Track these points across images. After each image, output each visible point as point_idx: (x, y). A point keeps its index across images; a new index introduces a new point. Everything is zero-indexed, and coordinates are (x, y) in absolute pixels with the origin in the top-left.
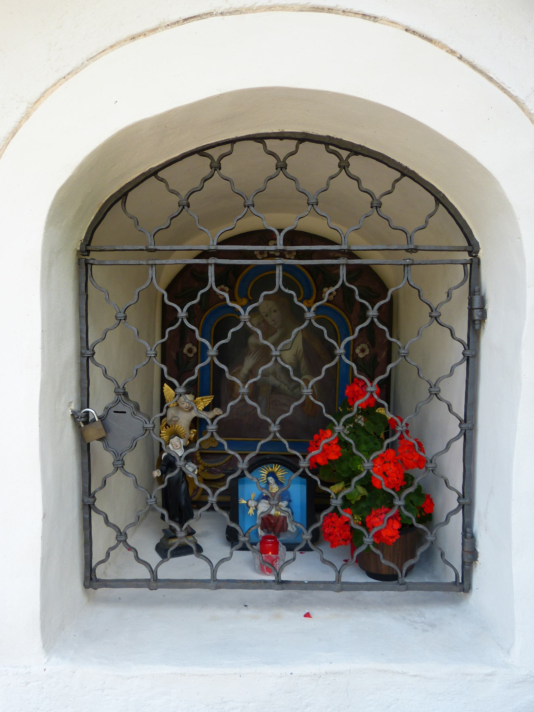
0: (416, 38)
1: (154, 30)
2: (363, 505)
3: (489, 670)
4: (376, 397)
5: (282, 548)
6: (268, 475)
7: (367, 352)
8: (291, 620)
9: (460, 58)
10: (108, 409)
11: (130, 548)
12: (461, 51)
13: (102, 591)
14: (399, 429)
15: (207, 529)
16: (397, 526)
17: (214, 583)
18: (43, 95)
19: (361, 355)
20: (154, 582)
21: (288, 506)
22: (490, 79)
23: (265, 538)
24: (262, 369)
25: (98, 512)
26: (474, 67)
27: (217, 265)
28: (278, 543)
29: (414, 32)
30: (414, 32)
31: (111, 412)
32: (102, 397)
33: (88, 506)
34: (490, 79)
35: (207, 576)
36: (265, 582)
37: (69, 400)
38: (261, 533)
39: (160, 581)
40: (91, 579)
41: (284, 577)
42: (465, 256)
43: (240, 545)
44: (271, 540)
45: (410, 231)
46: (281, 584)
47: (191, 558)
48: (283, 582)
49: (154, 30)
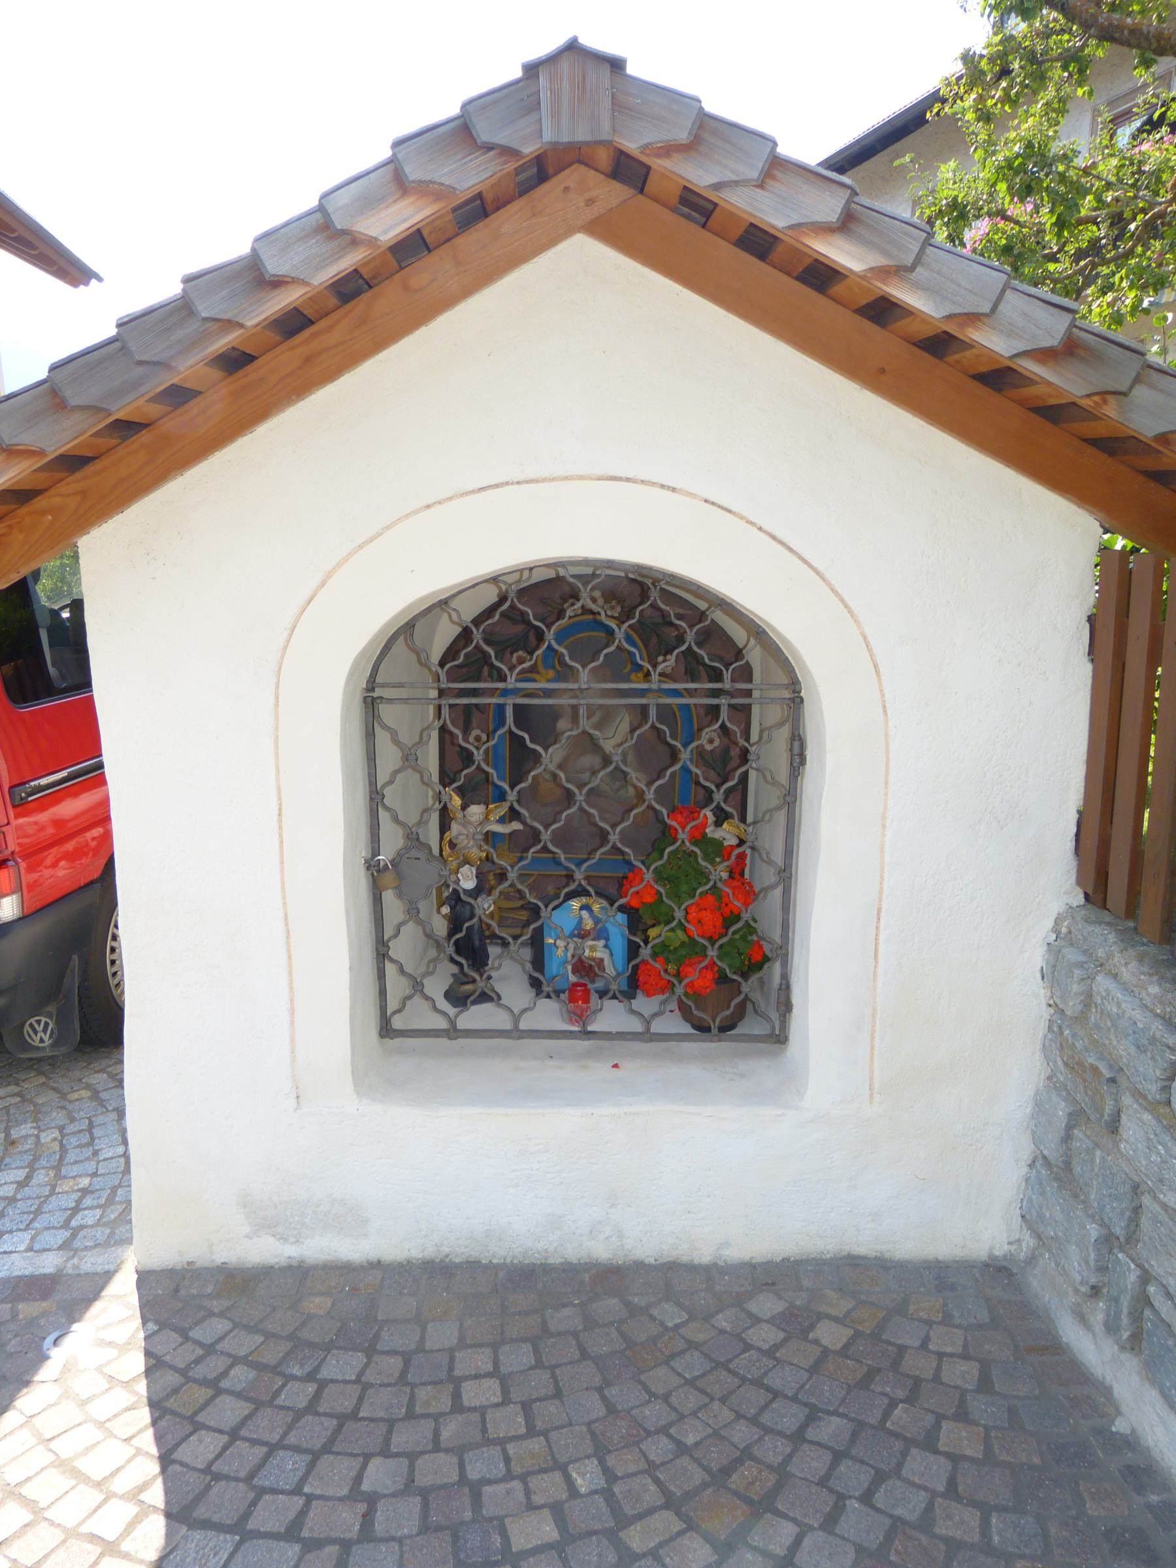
0: (715, 508)
1: (450, 499)
2: (683, 952)
3: (780, 1112)
4: (687, 844)
5: (594, 997)
6: (581, 908)
7: (717, 743)
8: (600, 1071)
9: (760, 529)
10: (399, 855)
11: (427, 998)
12: (760, 523)
13: (398, 1042)
14: (712, 877)
15: (508, 974)
16: (710, 976)
17: (516, 1033)
18: (339, 565)
19: (709, 747)
20: (453, 1032)
21: (606, 946)
22: (791, 550)
23: (575, 985)
24: (565, 814)
25: (392, 960)
26: (774, 538)
27: (515, 705)
28: (589, 991)
29: (713, 504)
30: (713, 504)
31: (404, 858)
32: (392, 843)
33: (382, 953)
34: (791, 550)
35: (508, 1026)
36: (571, 1032)
37: (363, 852)
38: (573, 979)
39: (460, 1031)
40: (386, 1030)
41: (590, 1028)
42: (787, 694)
43: (545, 994)
44: (581, 991)
45: (516, 1011)
46: (588, 1035)
47: (487, 1007)
48: (590, 1032)
49: (450, 499)
